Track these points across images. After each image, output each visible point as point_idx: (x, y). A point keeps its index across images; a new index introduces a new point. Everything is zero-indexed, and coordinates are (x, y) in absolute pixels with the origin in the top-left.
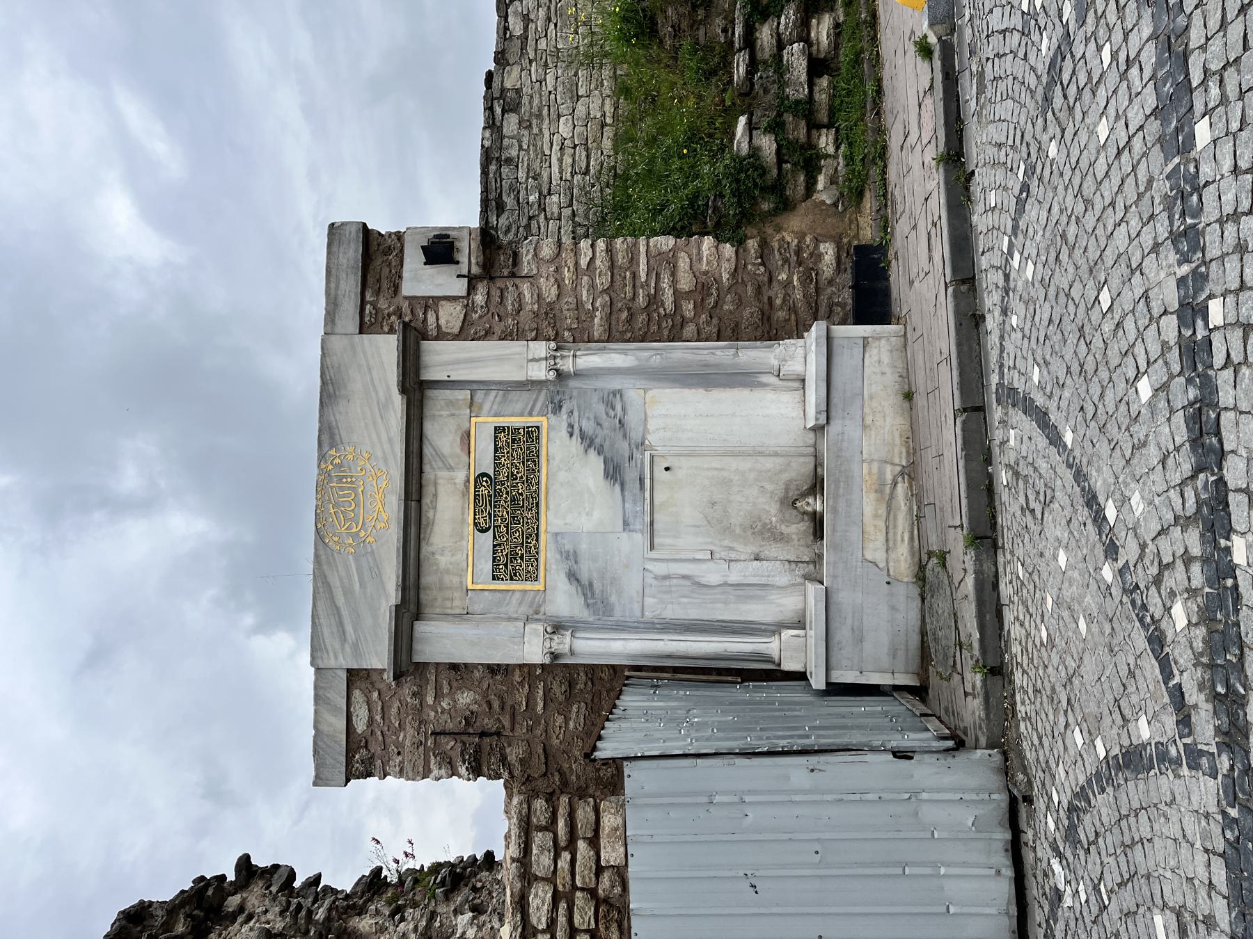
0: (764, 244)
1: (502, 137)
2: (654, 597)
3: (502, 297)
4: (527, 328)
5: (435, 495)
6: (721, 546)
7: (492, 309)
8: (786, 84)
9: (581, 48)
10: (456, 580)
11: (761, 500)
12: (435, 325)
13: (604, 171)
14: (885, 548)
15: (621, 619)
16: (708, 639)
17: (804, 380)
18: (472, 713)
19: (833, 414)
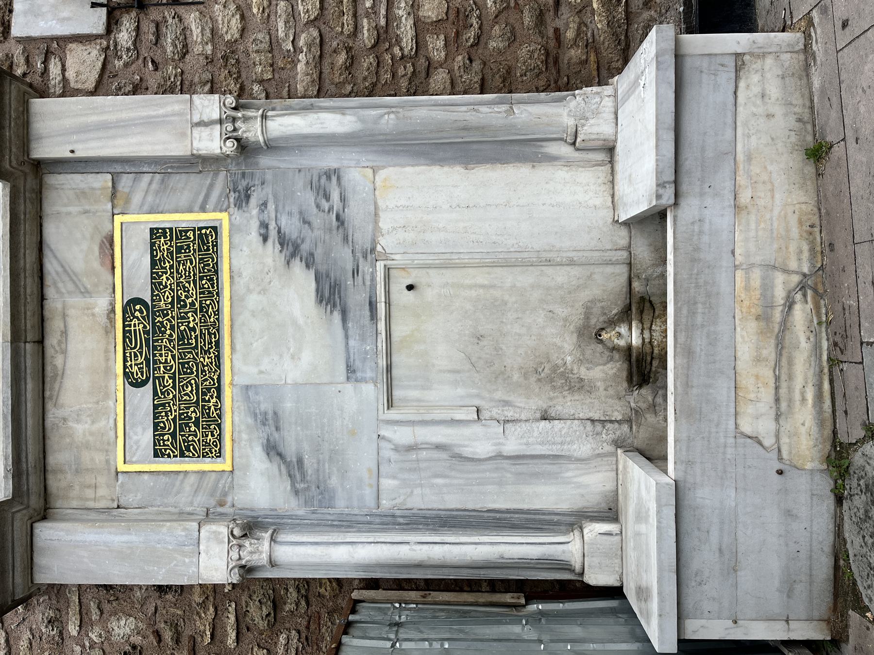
2: (394, 477)
4: (196, 79)
5: (65, 333)
6: (492, 400)
7: (144, 53)
10: (99, 458)
11: (550, 330)
12: (59, 78)
14: (773, 413)
15: (346, 511)
17: (611, 150)
18: (134, 647)
19: (684, 188)
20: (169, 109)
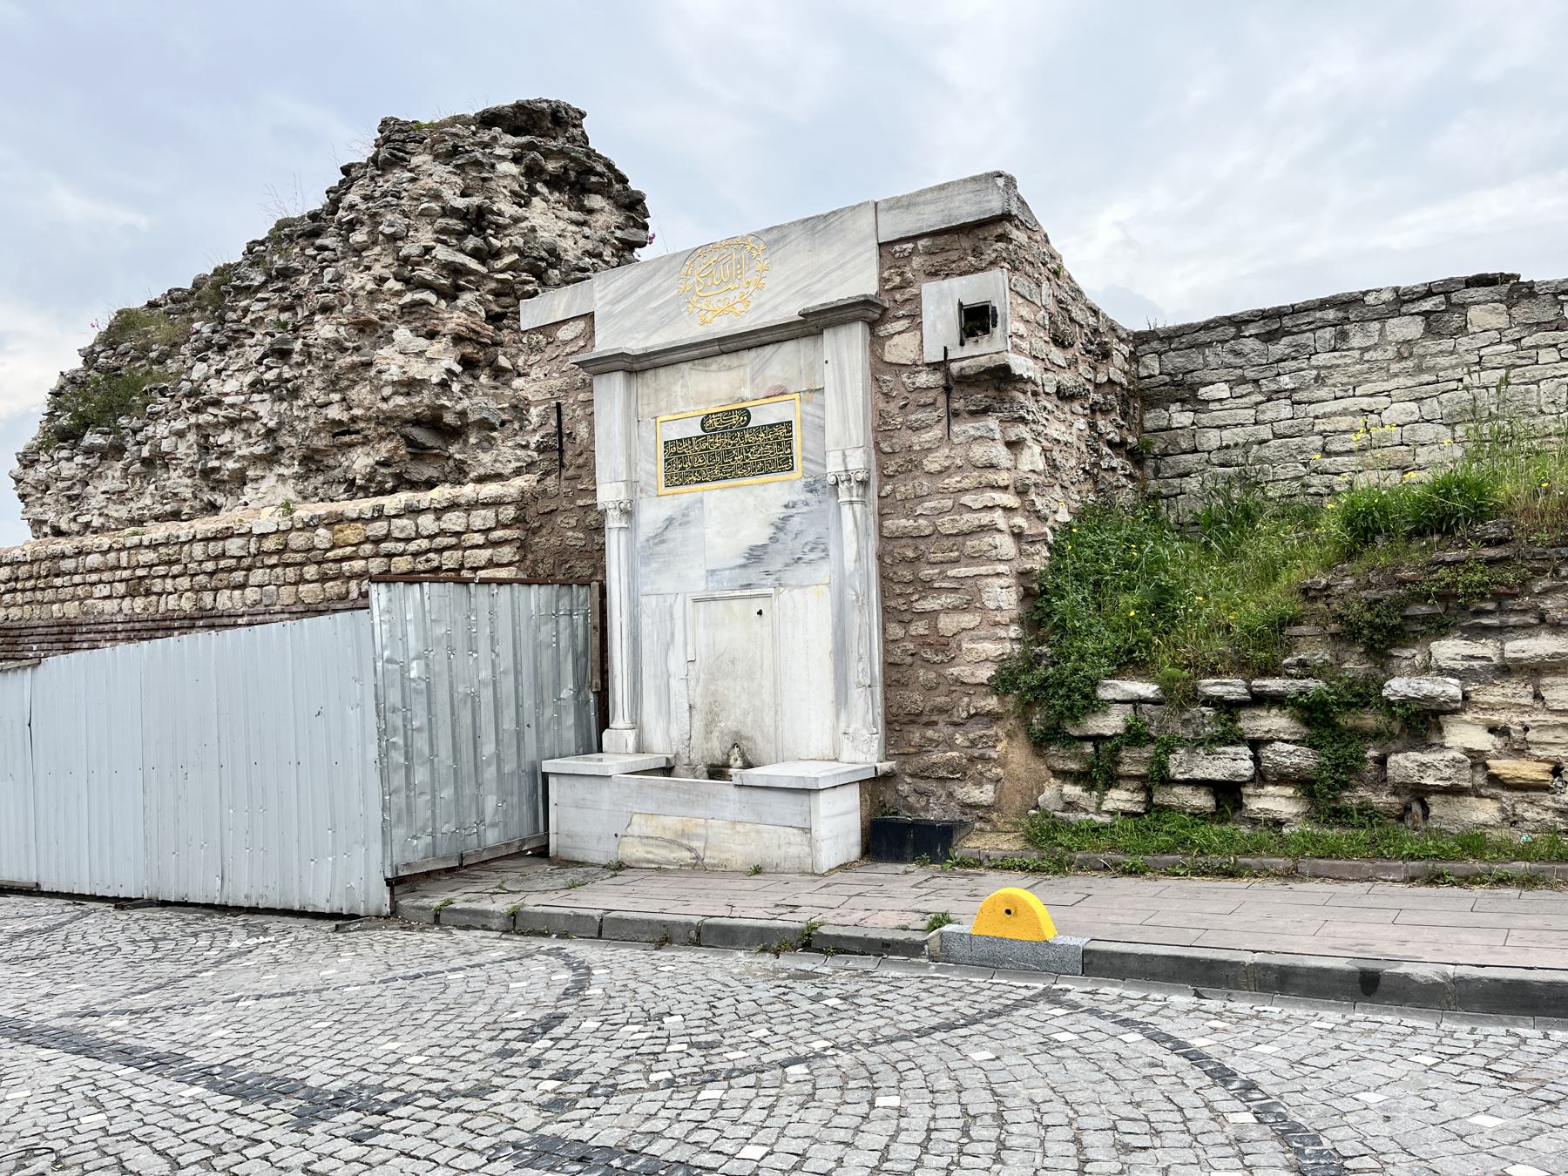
0: (993, 717)
1: (1382, 319)
3: (925, 406)
5: (730, 368)
7: (911, 397)
8: (1191, 752)
9: (1539, 420)
10: (663, 404)
13: (1326, 478)
16: (625, 659)
19: (744, 791)
20: (853, 431)
